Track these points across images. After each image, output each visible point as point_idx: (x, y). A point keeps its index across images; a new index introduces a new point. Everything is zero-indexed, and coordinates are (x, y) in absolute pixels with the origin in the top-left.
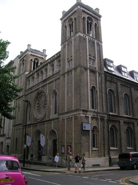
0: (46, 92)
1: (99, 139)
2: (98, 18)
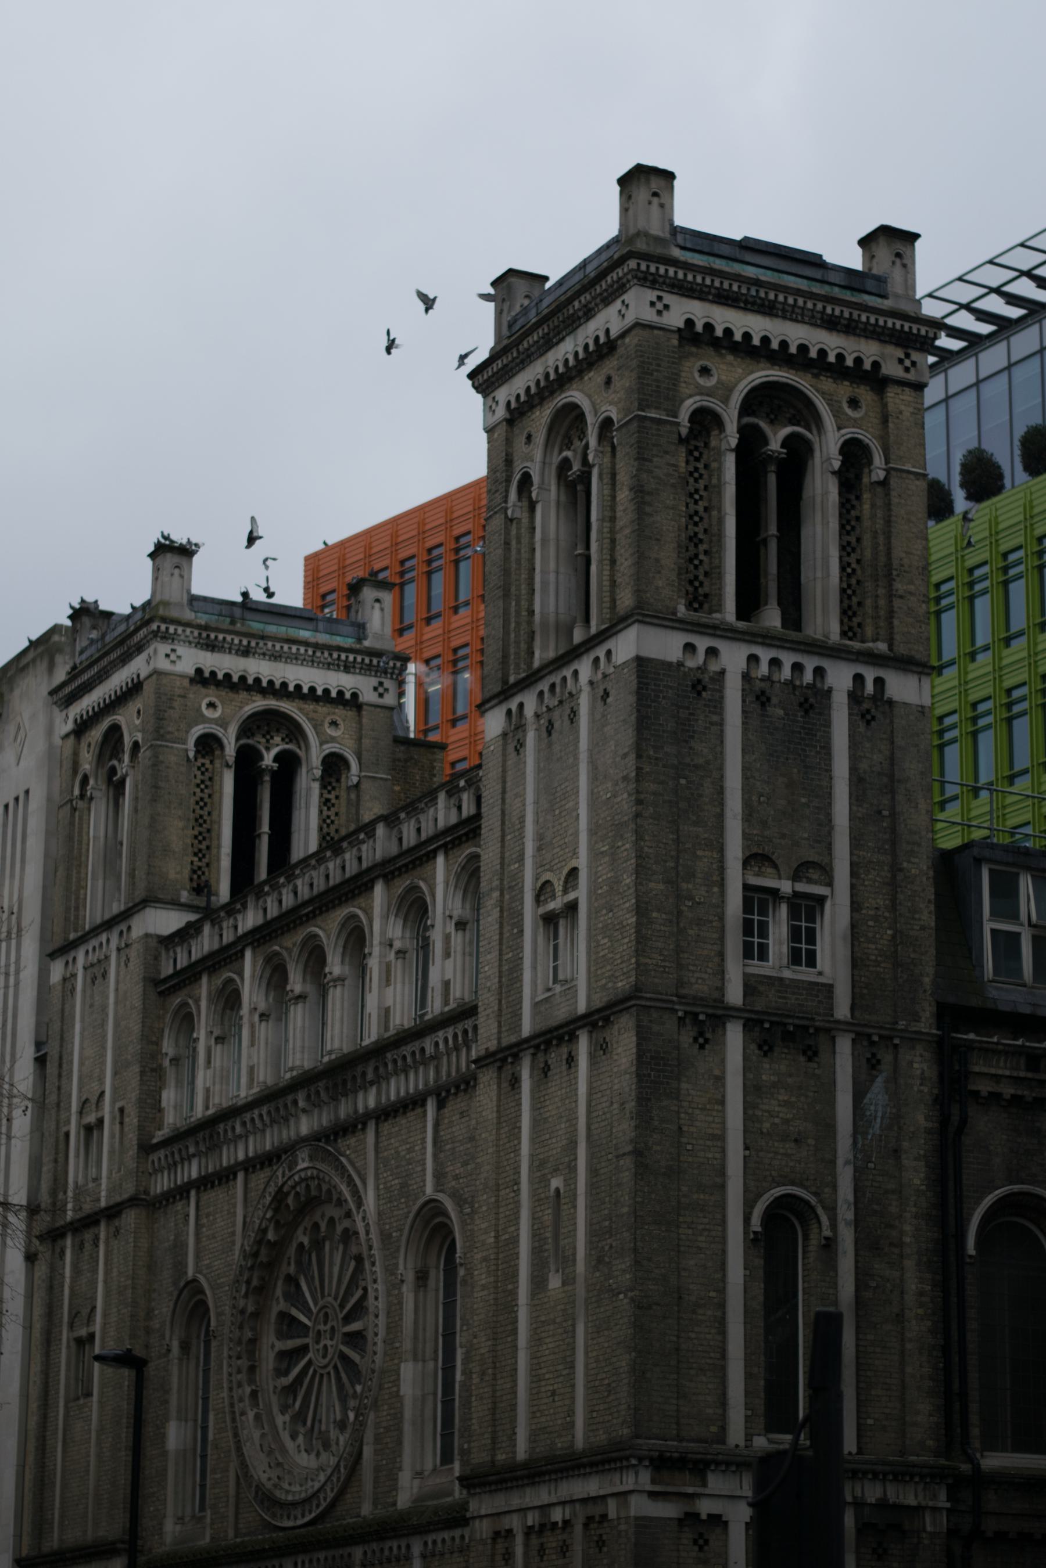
0: (352, 1206)
2: (891, 369)
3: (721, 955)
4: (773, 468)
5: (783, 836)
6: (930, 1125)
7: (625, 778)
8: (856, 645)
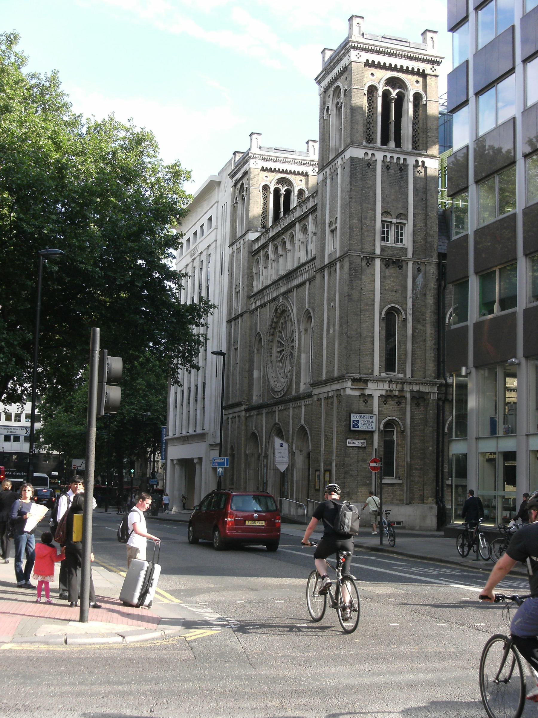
1: (402, 456)
3: (374, 240)
4: (393, 101)
5: (393, 206)
6: (435, 287)
7: (348, 191)
8: (417, 152)
